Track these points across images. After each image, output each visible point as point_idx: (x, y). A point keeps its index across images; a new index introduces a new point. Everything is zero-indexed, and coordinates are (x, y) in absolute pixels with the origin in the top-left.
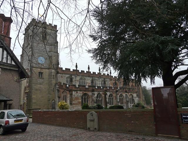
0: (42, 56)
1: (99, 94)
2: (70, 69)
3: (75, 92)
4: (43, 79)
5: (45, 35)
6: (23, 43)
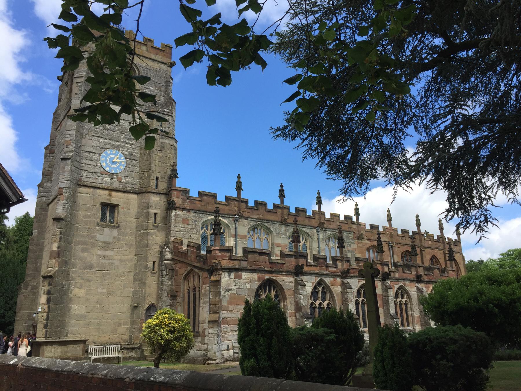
0: (117, 148)
1: (319, 283)
3: (232, 275)
4: (118, 227)
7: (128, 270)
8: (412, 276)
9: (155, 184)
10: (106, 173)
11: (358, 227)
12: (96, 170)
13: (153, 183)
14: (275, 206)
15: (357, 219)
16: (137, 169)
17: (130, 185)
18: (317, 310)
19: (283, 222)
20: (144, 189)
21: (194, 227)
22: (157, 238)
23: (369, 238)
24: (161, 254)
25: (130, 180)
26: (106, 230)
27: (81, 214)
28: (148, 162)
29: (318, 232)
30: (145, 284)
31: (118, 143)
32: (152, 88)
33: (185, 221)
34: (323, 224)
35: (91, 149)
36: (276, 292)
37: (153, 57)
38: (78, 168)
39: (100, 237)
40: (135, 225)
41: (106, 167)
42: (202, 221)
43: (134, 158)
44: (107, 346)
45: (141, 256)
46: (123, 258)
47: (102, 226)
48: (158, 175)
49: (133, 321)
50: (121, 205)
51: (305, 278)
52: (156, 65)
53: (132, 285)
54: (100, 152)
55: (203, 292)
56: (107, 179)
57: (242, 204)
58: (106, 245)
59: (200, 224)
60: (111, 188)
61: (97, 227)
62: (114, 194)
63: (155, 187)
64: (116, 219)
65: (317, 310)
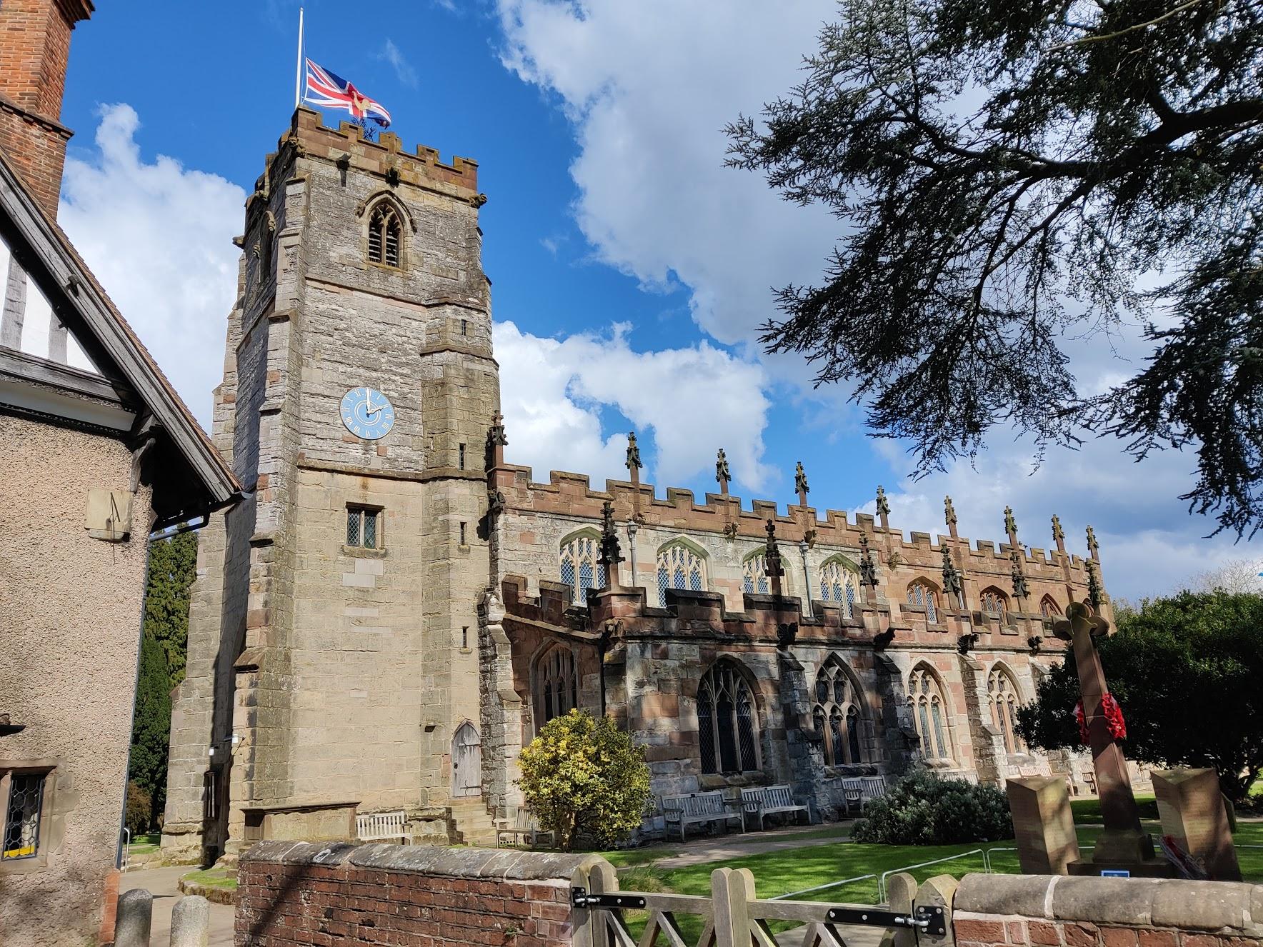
0: (374, 383)
1: (829, 662)
2: (584, 481)
4: (384, 555)
5: (394, 229)
6: (210, 726)
7: (410, 648)
8: (1022, 643)
9: (458, 460)
10: (352, 439)
11: (888, 539)
12: (333, 434)
13: (454, 459)
14: (711, 499)
15: (884, 522)
16: (418, 428)
17: (406, 464)
18: (827, 723)
19: (730, 533)
20: (437, 472)
21: (545, 549)
22: (471, 573)
23: (911, 561)
24: (482, 609)
25: (406, 452)
26: (359, 562)
27: (305, 530)
28: (442, 412)
29: (803, 552)
30: (447, 677)
31: (374, 374)
32: (440, 254)
33: (527, 537)
34: (813, 533)
35: (320, 390)
36: (741, 685)
37: (438, 187)
38: (295, 432)
39: (349, 580)
40: (419, 550)
41: (353, 426)
42: (562, 536)
43: (410, 405)
44: (377, 815)
45: (436, 618)
46: (398, 622)
47: (351, 554)
48: (463, 440)
49: (428, 759)
50: (389, 508)
51: (800, 653)
52: (446, 204)
53: (420, 681)
54: (339, 395)
55: (584, 689)
56: (356, 452)
57: (642, 496)
58: (360, 595)
59: (558, 542)
60: (366, 471)
61: (342, 557)
62: (372, 482)
63: (458, 466)
64: (379, 537)
65: (827, 723)
